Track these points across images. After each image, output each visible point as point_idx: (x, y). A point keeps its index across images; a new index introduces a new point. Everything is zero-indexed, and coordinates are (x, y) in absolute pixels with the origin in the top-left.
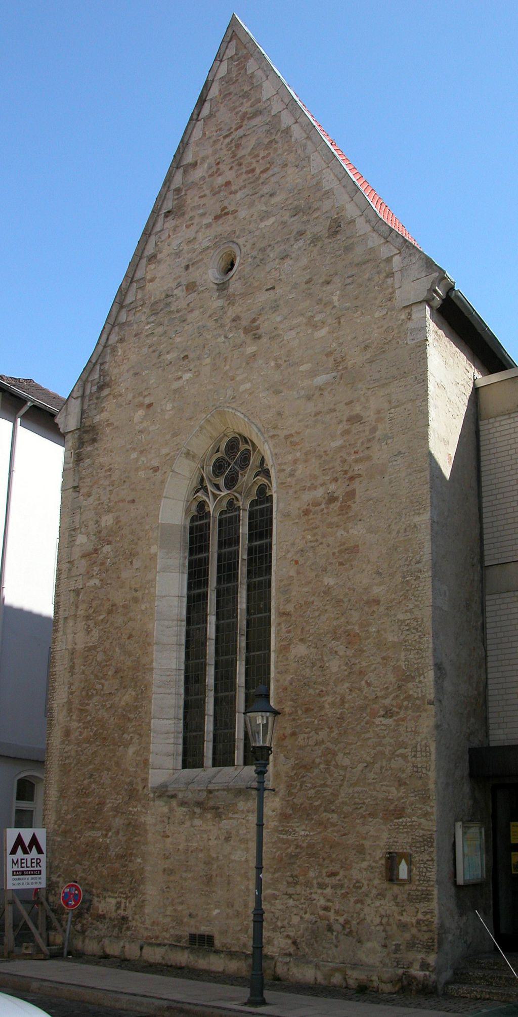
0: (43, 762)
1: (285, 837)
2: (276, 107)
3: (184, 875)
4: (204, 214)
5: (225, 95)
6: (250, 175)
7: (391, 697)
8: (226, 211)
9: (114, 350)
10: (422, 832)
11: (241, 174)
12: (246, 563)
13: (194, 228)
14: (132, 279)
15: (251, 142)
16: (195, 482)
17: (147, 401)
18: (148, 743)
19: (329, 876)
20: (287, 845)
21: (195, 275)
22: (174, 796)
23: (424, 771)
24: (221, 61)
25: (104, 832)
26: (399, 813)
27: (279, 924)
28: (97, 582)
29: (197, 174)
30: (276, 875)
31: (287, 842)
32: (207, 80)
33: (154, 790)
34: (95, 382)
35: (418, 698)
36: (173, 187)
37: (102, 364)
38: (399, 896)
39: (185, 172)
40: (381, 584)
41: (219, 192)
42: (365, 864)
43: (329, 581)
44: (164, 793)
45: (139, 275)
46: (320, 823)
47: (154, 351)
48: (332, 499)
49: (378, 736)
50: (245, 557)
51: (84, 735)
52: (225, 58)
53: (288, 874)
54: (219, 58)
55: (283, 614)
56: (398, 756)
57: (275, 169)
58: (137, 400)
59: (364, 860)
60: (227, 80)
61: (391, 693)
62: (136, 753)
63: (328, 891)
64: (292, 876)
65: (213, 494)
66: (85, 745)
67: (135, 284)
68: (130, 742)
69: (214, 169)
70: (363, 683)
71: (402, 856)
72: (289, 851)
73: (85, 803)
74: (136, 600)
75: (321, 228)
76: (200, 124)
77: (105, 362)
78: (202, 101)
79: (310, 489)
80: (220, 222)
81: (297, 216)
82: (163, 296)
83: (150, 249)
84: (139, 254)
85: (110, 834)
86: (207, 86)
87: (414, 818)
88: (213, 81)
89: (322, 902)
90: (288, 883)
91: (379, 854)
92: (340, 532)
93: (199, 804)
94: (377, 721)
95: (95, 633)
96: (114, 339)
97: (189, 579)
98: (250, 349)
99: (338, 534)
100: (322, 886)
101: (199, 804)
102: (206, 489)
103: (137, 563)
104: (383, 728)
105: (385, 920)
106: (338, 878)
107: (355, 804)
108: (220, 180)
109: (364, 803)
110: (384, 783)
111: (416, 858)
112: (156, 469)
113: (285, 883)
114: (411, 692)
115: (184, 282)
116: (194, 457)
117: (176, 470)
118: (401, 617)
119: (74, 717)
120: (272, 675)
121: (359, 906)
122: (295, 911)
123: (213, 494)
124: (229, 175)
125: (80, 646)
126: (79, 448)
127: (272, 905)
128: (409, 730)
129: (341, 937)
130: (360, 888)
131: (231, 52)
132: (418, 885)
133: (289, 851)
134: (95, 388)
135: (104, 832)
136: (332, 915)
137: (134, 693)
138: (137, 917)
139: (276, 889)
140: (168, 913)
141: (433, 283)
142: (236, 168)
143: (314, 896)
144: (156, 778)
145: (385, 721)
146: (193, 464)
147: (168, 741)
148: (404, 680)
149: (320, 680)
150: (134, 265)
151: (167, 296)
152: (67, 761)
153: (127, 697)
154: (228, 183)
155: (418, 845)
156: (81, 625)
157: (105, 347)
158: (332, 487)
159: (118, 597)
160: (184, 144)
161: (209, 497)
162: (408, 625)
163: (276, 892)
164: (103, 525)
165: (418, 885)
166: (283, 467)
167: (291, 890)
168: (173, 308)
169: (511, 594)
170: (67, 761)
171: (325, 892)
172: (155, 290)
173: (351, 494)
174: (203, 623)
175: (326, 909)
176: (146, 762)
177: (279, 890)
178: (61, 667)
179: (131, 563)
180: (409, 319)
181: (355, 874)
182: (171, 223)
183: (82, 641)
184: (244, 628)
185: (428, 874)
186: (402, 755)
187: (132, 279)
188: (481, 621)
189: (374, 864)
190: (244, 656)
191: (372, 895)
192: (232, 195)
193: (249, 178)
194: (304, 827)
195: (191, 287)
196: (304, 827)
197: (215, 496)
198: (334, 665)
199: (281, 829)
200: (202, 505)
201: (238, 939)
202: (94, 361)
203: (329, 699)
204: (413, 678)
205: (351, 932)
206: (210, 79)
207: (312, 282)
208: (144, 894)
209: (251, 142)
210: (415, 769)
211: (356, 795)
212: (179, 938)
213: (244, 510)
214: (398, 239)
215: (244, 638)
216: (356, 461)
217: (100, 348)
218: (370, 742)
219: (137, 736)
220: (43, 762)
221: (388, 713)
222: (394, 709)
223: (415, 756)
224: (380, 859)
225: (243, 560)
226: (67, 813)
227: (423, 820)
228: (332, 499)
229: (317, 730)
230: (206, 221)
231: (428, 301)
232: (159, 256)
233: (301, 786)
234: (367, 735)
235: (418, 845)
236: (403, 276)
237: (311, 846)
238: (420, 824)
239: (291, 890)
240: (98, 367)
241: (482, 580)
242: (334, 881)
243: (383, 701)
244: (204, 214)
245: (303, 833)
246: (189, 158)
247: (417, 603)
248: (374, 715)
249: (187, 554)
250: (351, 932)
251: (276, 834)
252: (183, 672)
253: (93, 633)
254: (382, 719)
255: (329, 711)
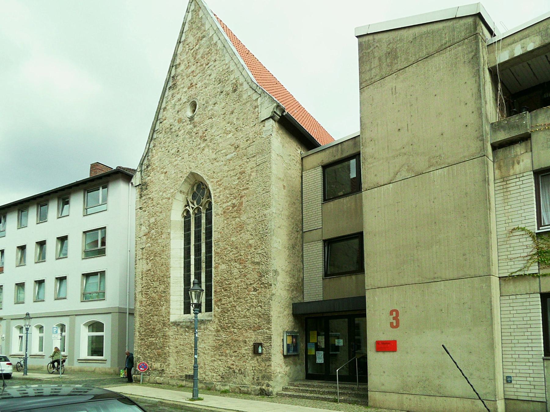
0: (133, 314)
1: (218, 338)
2: (211, 33)
3: (183, 353)
4: (183, 87)
5: (191, 29)
6: (201, 67)
7: (256, 283)
8: (192, 85)
9: (152, 150)
10: (267, 335)
11: (198, 67)
12: (205, 234)
13: (180, 94)
14: (157, 118)
15: (201, 51)
16: (186, 203)
17: (165, 171)
18: (169, 305)
19: (233, 352)
20: (219, 341)
21: (180, 115)
22: (179, 325)
23: (268, 312)
24: (189, 12)
25: (155, 339)
26: (259, 328)
27: (216, 370)
28: (150, 245)
29: (182, 67)
30: (215, 353)
31: (219, 340)
32: (183, 23)
33: (172, 323)
34: (145, 164)
35: (266, 284)
36: (172, 76)
37: (148, 157)
38: (259, 360)
39: (176, 68)
40: (252, 239)
41: (189, 76)
42: (246, 348)
43: (233, 239)
44: (176, 324)
45: (160, 116)
46: (230, 332)
47: (167, 150)
48: (234, 206)
49: (251, 299)
50: (204, 232)
51: (147, 303)
52: (190, 10)
53: (219, 352)
54: (188, 11)
55: (216, 253)
56: (258, 306)
57: (211, 63)
58: (161, 170)
59: (246, 346)
60: (192, 22)
61: (256, 282)
62: (166, 309)
63: (233, 358)
64: (220, 353)
65: (192, 207)
66: (147, 307)
67: (159, 121)
68: (163, 305)
69: (187, 66)
70: (246, 279)
71: (261, 344)
72: (219, 343)
73: (148, 328)
74: (163, 251)
75: (229, 88)
76: (181, 45)
77: (149, 156)
78: (182, 32)
79: (225, 203)
80: (190, 89)
81: (220, 84)
82: (169, 126)
83: (164, 105)
84: (159, 109)
85: (157, 339)
86: (184, 24)
87: (265, 330)
88: (186, 23)
89: (231, 362)
90: (219, 355)
91: (252, 343)
92: (237, 219)
93: (188, 327)
94: (251, 293)
95: (150, 265)
96: (152, 145)
97: (184, 242)
98: (202, 145)
99: (236, 220)
100: (231, 356)
101: (188, 327)
102: (189, 205)
103: (163, 236)
104: (253, 296)
105: (254, 368)
106: (237, 353)
107: (243, 325)
108: (190, 70)
109: (246, 325)
110: (254, 317)
111: (265, 345)
112: (169, 199)
113: (218, 355)
114: (263, 281)
115: (177, 119)
116: (183, 193)
117: (176, 198)
118: (260, 252)
119: (143, 297)
120: (213, 277)
121: (244, 363)
122: (221, 365)
123: (192, 207)
124: (193, 68)
125: (144, 270)
126: (141, 192)
127: (214, 363)
128: (263, 296)
129: (238, 375)
130: (245, 356)
131: (192, 7)
132: (266, 355)
133: (219, 343)
134: (146, 167)
135: (155, 339)
136: (234, 367)
137: (164, 287)
138: (167, 369)
139: (215, 358)
140: (178, 368)
141: (274, 109)
142: (196, 64)
143: (228, 360)
144: (173, 318)
145: (254, 293)
146: (183, 195)
147: (177, 304)
148: (261, 277)
149: (230, 278)
150: (158, 113)
151: (171, 125)
152: (142, 313)
153: (162, 288)
154: (193, 72)
155: (266, 340)
156: (145, 262)
157: (148, 149)
158: (234, 201)
159: (158, 249)
160: (175, 55)
161: (190, 208)
162: (263, 255)
163: (215, 359)
164: (151, 222)
165: (266, 355)
166: (216, 194)
167: (220, 358)
168: (173, 130)
169: (314, 243)
170: (142, 313)
171: (232, 358)
172: (166, 124)
173: (241, 204)
174: (188, 259)
175: (233, 365)
176: (169, 313)
177: (216, 358)
178: (138, 279)
179: (161, 236)
180: (264, 126)
181: (243, 351)
182: (171, 92)
183: (146, 267)
184: (205, 260)
185: (269, 351)
186: (260, 306)
187: (157, 118)
188: (301, 254)
189: (249, 348)
190: (205, 271)
191: (249, 359)
192: (195, 77)
193: (201, 68)
194: (224, 334)
195: (180, 121)
196: (224, 334)
197: (193, 208)
198: (235, 271)
199: (216, 335)
200: (188, 212)
201: (202, 376)
202: (144, 156)
203: (233, 285)
204: (264, 276)
205: (242, 373)
206: (184, 22)
207: (226, 114)
208: (169, 361)
209: (201, 51)
210: (265, 311)
211: (243, 322)
212: (181, 376)
213: (204, 213)
214: (260, 90)
215: (204, 264)
216: (243, 190)
217: (147, 150)
218: (248, 301)
219: (165, 303)
220: (133, 314)
221: (255, 290)
222: (257, 288)
223: (265, 306)
224: (252, 346)
225: (203, 233)
226: (143, 332)
227: (267, 331)
228: (234, 206)
229: (229, 297)
230: (184, 90)
231: (272, 117)
232: (167, 108)
233: (224, 319)
234: (247, 299)
235: (266, 340)
236: (261, 107)
237: (227, 341)
238: (266, 332)
239: (220, 358)
240: (146, 158)
241: (302, 237)
242: (235, 354)
243: (253, 285)
244: (183, 87)
245: (224, 336)
246: (178, 61)
247: (265, 246)
248: (249, 291)
249: (183, 232)
250: (242, 373)
251: (215, 337)
252: (183, 278)
253: (149, 264)
254: (252, 292)
255: (234, 290)
